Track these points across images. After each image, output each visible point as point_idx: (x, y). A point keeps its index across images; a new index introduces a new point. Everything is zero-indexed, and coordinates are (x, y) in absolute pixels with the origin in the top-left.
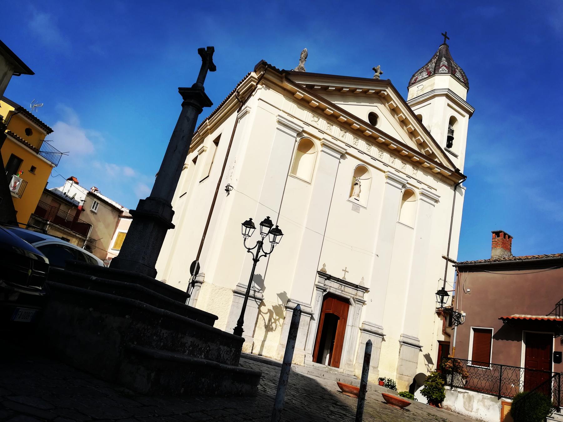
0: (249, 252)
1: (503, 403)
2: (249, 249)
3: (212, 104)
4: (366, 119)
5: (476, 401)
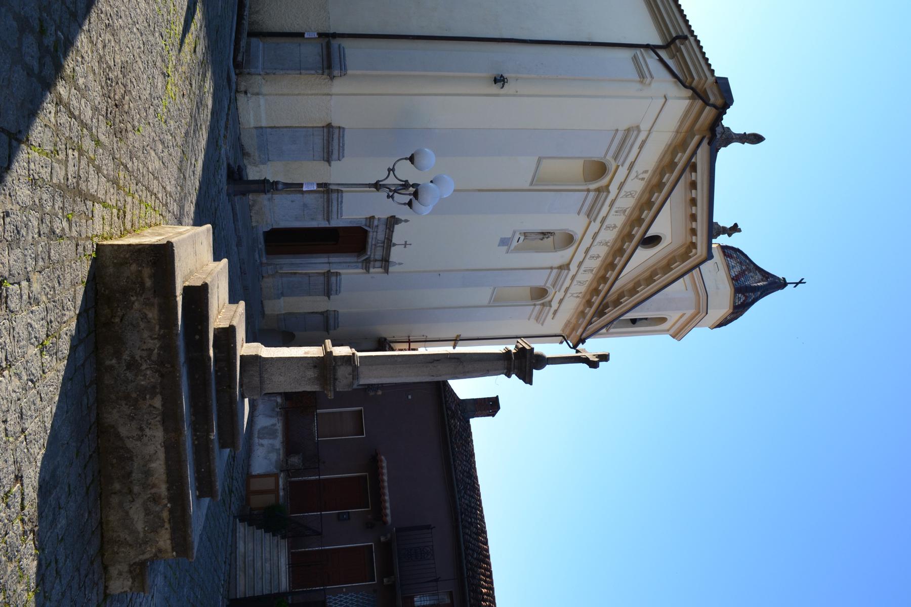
0: (389, 170)
1: (276, 476)
2: (393, 170)
3: (497, 398)
4: (651, 232)
5: (271, 441)
